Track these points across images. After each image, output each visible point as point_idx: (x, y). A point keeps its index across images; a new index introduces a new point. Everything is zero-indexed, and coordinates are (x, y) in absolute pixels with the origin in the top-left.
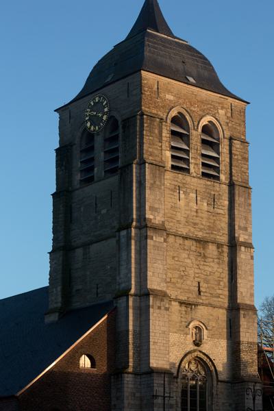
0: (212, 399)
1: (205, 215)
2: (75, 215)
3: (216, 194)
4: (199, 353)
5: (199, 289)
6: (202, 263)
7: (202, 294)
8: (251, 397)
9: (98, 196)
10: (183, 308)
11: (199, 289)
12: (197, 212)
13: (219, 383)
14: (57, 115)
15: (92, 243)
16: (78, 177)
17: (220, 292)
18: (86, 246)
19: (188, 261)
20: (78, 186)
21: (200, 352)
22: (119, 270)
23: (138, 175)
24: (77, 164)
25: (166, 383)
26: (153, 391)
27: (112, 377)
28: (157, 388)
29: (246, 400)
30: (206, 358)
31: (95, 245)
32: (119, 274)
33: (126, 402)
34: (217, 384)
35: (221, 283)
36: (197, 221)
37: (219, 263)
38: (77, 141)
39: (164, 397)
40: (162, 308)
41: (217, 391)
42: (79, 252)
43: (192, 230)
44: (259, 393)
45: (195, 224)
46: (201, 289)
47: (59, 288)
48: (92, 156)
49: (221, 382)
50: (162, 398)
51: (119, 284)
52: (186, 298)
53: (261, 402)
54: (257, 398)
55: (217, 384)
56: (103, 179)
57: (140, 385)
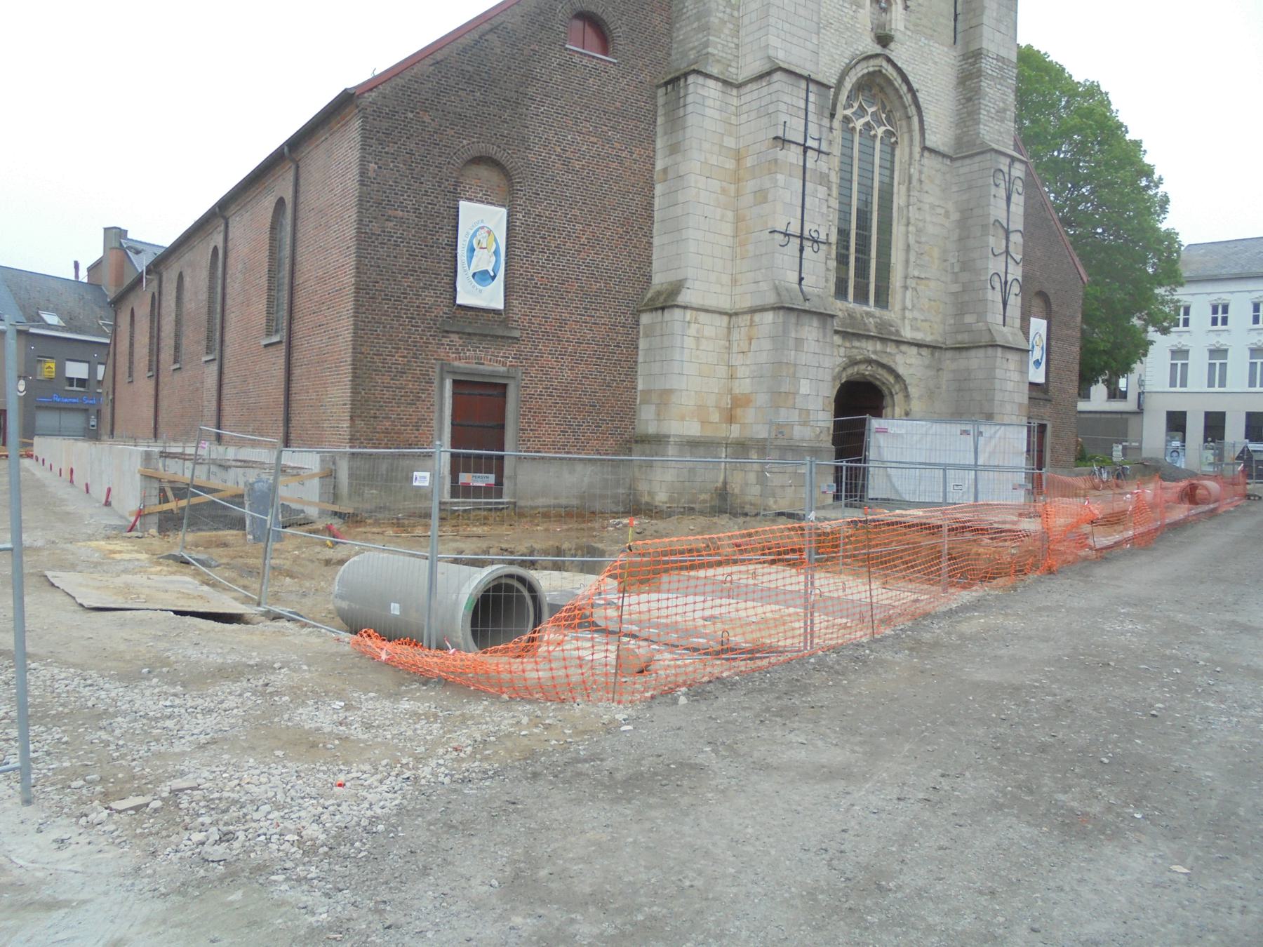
0: (909, 190)
4: (884, 64)
8: (1002, 193)
13: (926, 154)
21: (889, 60)
25: (811, 107)
27: (661, 91)
28: (787, 118)
29: (992, 199)
30: (899, 80)
34: (922, 155)
39: (806, 149)
41: (921, 172)
44: (1019, 186)
48: (916, 406)
49: (931, 150)
53: (1021, 210)
54: (1015, 197)
55: (922, 155)
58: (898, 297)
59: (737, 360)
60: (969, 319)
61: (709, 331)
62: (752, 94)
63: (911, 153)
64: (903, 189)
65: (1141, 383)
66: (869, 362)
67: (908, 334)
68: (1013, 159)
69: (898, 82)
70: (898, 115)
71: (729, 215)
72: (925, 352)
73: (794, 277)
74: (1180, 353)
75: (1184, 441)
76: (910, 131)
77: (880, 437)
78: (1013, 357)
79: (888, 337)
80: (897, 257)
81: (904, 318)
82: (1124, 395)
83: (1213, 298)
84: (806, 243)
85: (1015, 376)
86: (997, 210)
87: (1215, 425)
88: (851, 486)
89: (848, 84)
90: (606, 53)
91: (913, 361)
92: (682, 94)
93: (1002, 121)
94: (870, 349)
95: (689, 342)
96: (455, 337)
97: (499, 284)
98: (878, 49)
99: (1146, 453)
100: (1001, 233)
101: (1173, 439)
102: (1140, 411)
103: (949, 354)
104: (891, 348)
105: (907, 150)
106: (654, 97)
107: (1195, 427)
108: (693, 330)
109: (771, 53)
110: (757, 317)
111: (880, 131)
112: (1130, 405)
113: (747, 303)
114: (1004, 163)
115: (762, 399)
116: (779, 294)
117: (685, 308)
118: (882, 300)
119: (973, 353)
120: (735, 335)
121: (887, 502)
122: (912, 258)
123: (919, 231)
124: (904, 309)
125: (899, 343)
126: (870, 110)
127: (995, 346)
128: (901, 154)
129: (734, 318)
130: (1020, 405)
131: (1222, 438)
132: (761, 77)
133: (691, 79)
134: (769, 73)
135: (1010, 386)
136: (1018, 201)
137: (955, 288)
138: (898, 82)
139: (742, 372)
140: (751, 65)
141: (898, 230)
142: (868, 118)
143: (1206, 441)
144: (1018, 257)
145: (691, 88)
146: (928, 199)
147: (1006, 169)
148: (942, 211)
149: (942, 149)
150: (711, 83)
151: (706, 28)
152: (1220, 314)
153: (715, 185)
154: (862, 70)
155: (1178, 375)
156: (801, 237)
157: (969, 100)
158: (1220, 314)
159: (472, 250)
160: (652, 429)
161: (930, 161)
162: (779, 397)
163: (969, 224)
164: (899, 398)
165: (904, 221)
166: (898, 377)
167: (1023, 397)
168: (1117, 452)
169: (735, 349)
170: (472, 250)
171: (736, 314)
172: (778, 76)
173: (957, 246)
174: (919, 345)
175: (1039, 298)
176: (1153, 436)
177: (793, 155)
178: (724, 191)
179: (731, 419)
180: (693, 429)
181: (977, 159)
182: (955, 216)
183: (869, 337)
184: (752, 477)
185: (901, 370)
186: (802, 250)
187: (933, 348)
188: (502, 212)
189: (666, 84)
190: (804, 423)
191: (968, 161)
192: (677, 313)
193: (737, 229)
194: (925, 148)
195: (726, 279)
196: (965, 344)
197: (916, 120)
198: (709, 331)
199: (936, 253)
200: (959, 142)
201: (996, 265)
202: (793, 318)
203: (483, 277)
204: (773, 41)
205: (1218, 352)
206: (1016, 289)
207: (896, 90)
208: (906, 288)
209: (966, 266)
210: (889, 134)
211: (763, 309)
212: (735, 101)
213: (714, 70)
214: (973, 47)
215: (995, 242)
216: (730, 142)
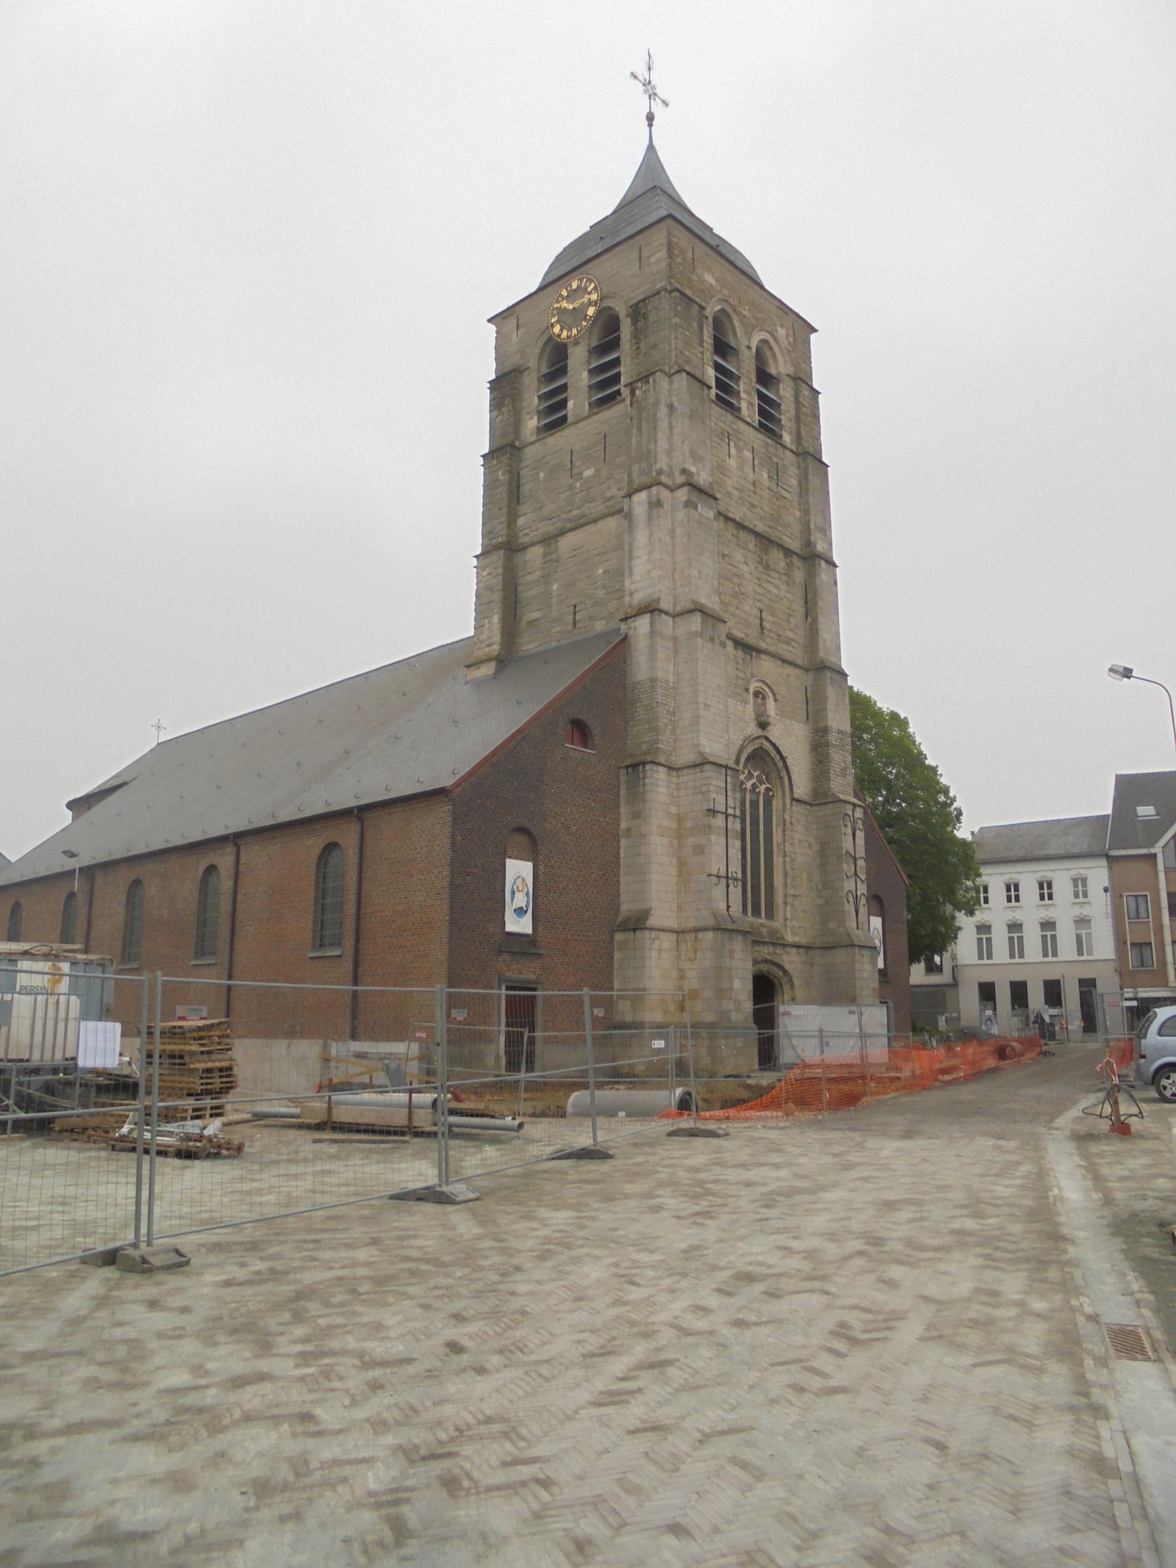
0: (784, 830)
1: (766, 494)
2: (526, 488)
3: (780, 463)
4: (764, 742)
5: (761, 624)
6: (765, 577)
7: (766, 632)
8: (850, 831)
9: (576, 448)
10: (740, 654)
11: (761, 624)
12: (754, 484)
14: (493, 328)
15: (563, 533)
16: (532, 423)
17: (790, 634)
18: (548, 540)
19: (745, 568)
20: (534, 438)
21: (767, 739)
22: (630, 568)
23: (169, 1096)
24: (532, 399)
25: (729, 786)
26: (708, 801)
31: (570, 535)
32: (631, 574)
33: (655, 821)
35: (792, 620)
36: (756, 503)
37: (787, 584)
38: (532, 363)
39: (727, 816)
40: (717, 641)
41: (791, 817)
42: (535, 554)
43: (749, 514)
44: (860, 825)
45: (753, 505)
46: (765, 624)
47: (496, 619)
48: (799, 993)
49: (798, 801)
50: (723, 817)
51: (631, 594)
52: (743, 636)
56: (587, 417)
57: (678, 789)
58: (781, 910)
59: (686, 965)
60: (832, 925)
61: (666, 945)
62: (687, 777)
63: (784, 803)
64: (780, 829)
65: (954, 957)
66: (766, 961)
67: (790, 938)
68: (855, 805)
69: (773, 753)
70: (774, 775)
71: (674, 860)
72: (801, 951)
73: (723, 906)
74: (983, 928)
75: (995, 1009)
76: (783, 787)
77: (785, 1018)
78: (866, 953)
79: (777, 941)
80: (778, 880)
81: (786, 926)
82: (939, 969)
83: (1006, 877)
84: (730, 882)
85: (868, 967)
86: (847, 844)
87: (1019, 992)
88: (767, 1054)
89: (743, 760)
90: (585, 746)
91: (794, 959)
92: (641, 776)
93: (844, 776)
94: (765, 951)
95: (654, 954)
96: (506, 955)
97: (529, 917)
98: (760, 732)
99: (963, 1024)
100: (851, 860)
101: (986, 1008)
102: (955, 984)
103: (817, 952)
104: (779, 950)
105: (781, 801)
106: (618, 776)
107: (1003, 996)
108: (656, 944)
109: (702, 749)
110: (700, 935)
111: (762, 788)
112: (945, 978)
113: (692, 924)
114: (849, 810)
115: (708, 993)
116: (716, 918)
117: (651, 929)
118: (770, 915)
119: (837, 951)
120: (683, 947)
121: (791, 1067)
122: (789, 881)
123: (793, 860)
124: (786, 919)
125: (784, 946)
126: (756, 774)
127: (853, 946)
128: (776, 804)
129: (681, 936)
130: (874, 989)
131: (1027, 1006)
132: (696, 766)
133: (648, 767)
134: (701, 764)
135: (866, 975)
136: (860, 835)
137: (819, 901)
138: (773, 753)
139: (690, 974)
140: (686, 756)
141: (778, 860)
142: (754, 780)
143: (1013, 1008)
144: (863, 877)
145: (649, 774)
146: (798, 836)
147: (850, 813)
148: (806, 844)
149: (805, 798)
150: (661, 769)
151: (656, 730)
152: (1013, 891)
153: (666, 840)
154: (750, 749)
155: (985, 948)
156: (727, 877)
157: (821, 762)
158: (1013, 891)
159: (513, 893)
160: (628, 1018)
161: (797, 808)
162: (721, 992)
163: (827, 853)
164: (786, 987)
165: (782, 854)
166: (785, 972)
167: (874, 983)
168: (942, 1022)
169: (683, 957)
170: (513, 893)
171: (683, 932)
172: (707, 767)
173: (823, 871)
174: (798, 946)
175: (877, 902)
176: (969, 1003)
177: (719, 821)
178: (671, 845)
179: (682, 1009)
180: (658, 1017)
181: (830, 806)
182: (816, 847)
183: (764, 943)
184: (703, 1051)
185: (787, 966)
186: (728, 887)
187: (808, 948)
188: (530, 865)
189: (627, 767)
190: (737, 1010)
191: (822, 808)
192: (647, 933)
193: (680, 871)
194: (793, 799)
195: (675, 907)
196: (831, 944)
197: (786, 779)
198: (666, 945)
199: (805, 876)
200: (816, 793)
201: (849, 885)
202: (727, 935)
203: (520, 912)
204: (703, 741)
205: (1015, 927)
206: (863, 901)
207: (773, 759)
208: (786, 903)
209: (827, 886)
210: (768, 789)
211: (705, 929)
212: (675, 780)
213: (662, 760)
214: (822, 725)
215: (847, 868)
216: (673, 810)
